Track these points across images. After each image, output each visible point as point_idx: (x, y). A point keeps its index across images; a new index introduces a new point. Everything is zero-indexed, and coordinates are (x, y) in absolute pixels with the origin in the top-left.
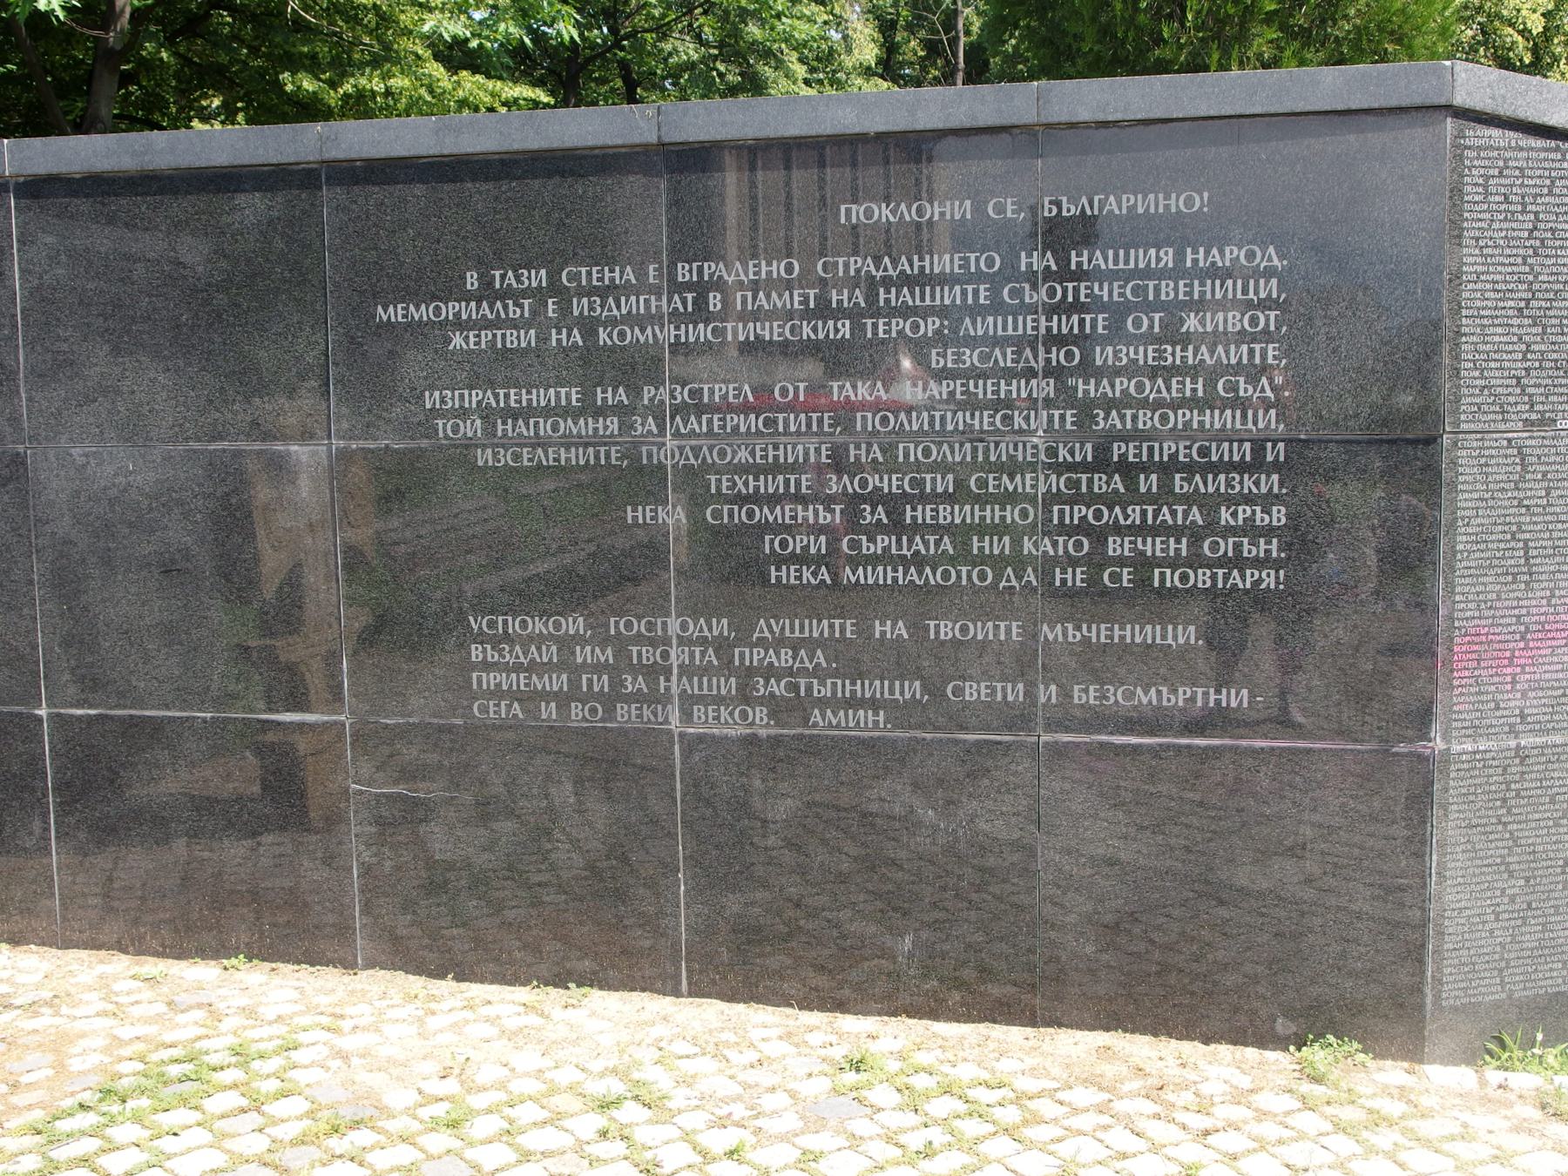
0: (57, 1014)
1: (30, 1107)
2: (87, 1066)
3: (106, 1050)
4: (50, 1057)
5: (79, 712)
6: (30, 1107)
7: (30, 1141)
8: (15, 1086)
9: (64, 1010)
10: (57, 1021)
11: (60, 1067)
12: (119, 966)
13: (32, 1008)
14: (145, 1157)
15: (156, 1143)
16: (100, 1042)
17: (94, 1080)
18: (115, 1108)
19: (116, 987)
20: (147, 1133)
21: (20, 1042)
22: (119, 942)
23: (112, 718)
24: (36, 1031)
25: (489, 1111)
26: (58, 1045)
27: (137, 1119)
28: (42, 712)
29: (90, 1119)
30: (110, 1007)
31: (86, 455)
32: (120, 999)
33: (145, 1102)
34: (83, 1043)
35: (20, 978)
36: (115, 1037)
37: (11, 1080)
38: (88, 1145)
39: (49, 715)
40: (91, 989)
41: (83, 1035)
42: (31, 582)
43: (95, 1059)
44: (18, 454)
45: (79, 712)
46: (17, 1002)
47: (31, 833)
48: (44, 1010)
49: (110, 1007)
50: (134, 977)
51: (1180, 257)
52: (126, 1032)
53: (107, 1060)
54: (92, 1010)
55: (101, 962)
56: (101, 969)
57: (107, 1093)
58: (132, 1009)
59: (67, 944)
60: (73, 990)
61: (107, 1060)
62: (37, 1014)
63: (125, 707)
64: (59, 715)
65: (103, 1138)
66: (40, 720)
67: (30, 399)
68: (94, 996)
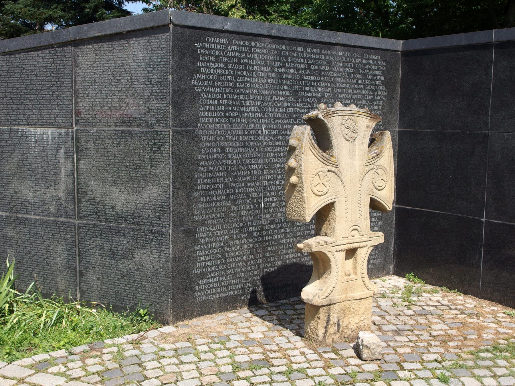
0: (479, 319)
1: (470, 346)
2: (488, 338)
3: (494, 334)
4: (477, 332)
5: (496, 221)
6: (470, 346)
7: (470, 356)
8: (465, 338)
9: (481, 318)
10: (479, 321)
11: (480, 336)
12: (498, 308)
13: (471, 315)
14: (508, 372)
15: (512, 369)
16: (492, 331)
17: (491, 343)
18: (498, 354)
19: (498, 315)
20: (508, 365)
21: (467, 325)
22: (500, 300)
23: (507, 225)
24: (471, 323)
25: (245, 379)
26: (479, 329)
27: (505, 359)
28: (483, 220)
29: (490, 355)
30: (496, 321)
31: (509, 136)
32: (500, 319)
33: (508, 354)
34: (488, 330)
35: (467, 305)
36: (498, 331)
37: (464, 336)
38: (489, 363)
39: (485, 221)
40: (489, 314)
41: (487, 328)
42: (485, 177)
43: (490, 336)
44: (486, 134)
45: (496, 221)
46: (466, 312)
47: (475, 259)
48: (474, 317)
49: (496, 321)
50: (504, 313)
51: (234, 293)
52: (502, 330)
53: (495, 337)
54: (490, 320)
55: (493, 306)
56: (492, 308)
57: (495, 348)
58: (503, 323)
59: (482, 298)
60: (484, 313)
61: (495, 337)
62: (472, 318)
63: (512, 222)
64: (489, 221)
65: (494, 362)
66: (482, 222)
67: (492, 116)
68: (490, 316)
